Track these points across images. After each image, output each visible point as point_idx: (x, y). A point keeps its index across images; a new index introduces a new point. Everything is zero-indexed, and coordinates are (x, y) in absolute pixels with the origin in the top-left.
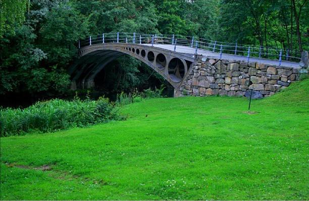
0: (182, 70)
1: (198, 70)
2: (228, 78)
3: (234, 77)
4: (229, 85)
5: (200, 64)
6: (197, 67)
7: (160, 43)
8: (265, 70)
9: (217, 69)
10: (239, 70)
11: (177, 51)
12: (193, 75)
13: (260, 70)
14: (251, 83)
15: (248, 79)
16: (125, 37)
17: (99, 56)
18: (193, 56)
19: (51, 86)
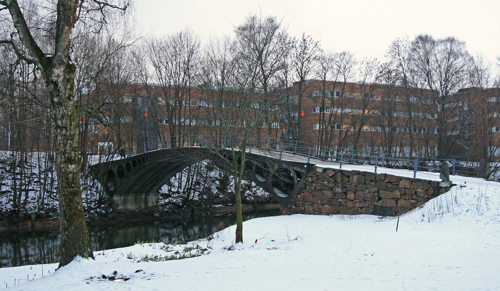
0: (412, 208)
1: (312, 183)
2: (350, 192)
3: (358, 191)
4: (352, 201)
5: (315, 175)
6: (310, 179)
7: (398, 167)
8: (397, 183)
9: (336, 181)
10: (365, 183)
11: (417, 177)
12: (306, 188)
13: (391, 183)
14: (380, 199)
15: (376, 194)
16: (297, 146)
17: (170, 162)
18: (305, 166)
19: (182, 225)
